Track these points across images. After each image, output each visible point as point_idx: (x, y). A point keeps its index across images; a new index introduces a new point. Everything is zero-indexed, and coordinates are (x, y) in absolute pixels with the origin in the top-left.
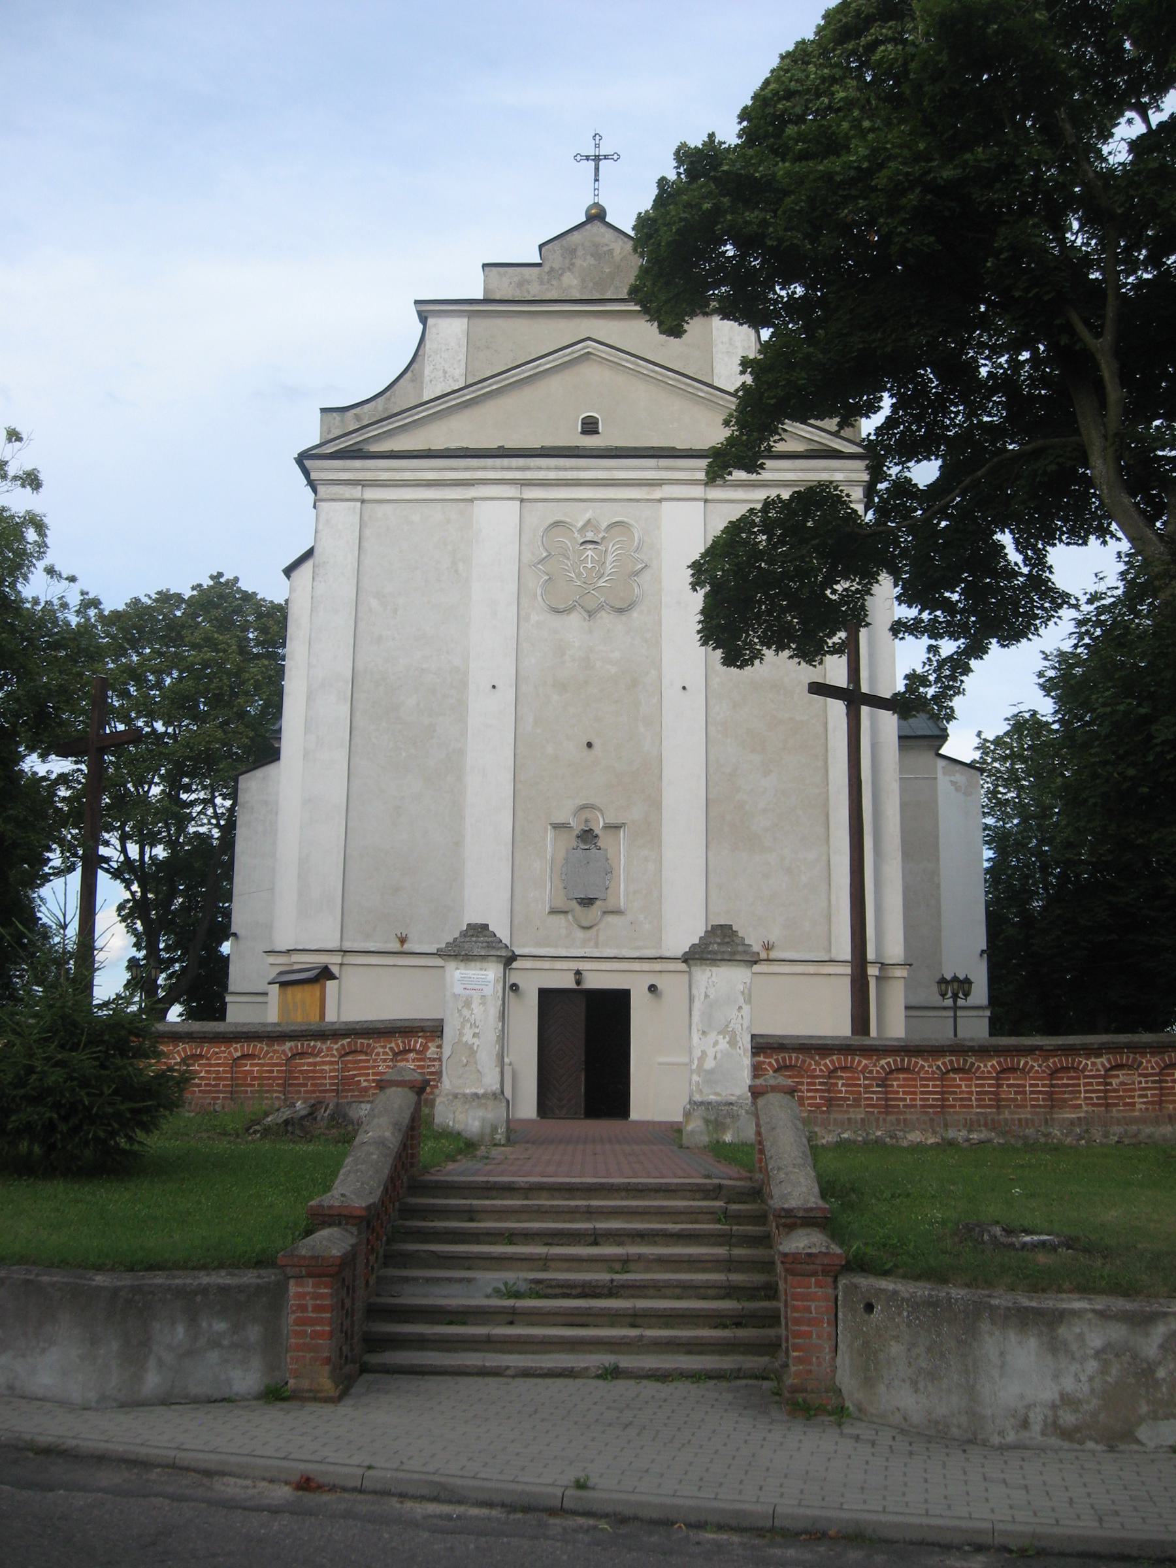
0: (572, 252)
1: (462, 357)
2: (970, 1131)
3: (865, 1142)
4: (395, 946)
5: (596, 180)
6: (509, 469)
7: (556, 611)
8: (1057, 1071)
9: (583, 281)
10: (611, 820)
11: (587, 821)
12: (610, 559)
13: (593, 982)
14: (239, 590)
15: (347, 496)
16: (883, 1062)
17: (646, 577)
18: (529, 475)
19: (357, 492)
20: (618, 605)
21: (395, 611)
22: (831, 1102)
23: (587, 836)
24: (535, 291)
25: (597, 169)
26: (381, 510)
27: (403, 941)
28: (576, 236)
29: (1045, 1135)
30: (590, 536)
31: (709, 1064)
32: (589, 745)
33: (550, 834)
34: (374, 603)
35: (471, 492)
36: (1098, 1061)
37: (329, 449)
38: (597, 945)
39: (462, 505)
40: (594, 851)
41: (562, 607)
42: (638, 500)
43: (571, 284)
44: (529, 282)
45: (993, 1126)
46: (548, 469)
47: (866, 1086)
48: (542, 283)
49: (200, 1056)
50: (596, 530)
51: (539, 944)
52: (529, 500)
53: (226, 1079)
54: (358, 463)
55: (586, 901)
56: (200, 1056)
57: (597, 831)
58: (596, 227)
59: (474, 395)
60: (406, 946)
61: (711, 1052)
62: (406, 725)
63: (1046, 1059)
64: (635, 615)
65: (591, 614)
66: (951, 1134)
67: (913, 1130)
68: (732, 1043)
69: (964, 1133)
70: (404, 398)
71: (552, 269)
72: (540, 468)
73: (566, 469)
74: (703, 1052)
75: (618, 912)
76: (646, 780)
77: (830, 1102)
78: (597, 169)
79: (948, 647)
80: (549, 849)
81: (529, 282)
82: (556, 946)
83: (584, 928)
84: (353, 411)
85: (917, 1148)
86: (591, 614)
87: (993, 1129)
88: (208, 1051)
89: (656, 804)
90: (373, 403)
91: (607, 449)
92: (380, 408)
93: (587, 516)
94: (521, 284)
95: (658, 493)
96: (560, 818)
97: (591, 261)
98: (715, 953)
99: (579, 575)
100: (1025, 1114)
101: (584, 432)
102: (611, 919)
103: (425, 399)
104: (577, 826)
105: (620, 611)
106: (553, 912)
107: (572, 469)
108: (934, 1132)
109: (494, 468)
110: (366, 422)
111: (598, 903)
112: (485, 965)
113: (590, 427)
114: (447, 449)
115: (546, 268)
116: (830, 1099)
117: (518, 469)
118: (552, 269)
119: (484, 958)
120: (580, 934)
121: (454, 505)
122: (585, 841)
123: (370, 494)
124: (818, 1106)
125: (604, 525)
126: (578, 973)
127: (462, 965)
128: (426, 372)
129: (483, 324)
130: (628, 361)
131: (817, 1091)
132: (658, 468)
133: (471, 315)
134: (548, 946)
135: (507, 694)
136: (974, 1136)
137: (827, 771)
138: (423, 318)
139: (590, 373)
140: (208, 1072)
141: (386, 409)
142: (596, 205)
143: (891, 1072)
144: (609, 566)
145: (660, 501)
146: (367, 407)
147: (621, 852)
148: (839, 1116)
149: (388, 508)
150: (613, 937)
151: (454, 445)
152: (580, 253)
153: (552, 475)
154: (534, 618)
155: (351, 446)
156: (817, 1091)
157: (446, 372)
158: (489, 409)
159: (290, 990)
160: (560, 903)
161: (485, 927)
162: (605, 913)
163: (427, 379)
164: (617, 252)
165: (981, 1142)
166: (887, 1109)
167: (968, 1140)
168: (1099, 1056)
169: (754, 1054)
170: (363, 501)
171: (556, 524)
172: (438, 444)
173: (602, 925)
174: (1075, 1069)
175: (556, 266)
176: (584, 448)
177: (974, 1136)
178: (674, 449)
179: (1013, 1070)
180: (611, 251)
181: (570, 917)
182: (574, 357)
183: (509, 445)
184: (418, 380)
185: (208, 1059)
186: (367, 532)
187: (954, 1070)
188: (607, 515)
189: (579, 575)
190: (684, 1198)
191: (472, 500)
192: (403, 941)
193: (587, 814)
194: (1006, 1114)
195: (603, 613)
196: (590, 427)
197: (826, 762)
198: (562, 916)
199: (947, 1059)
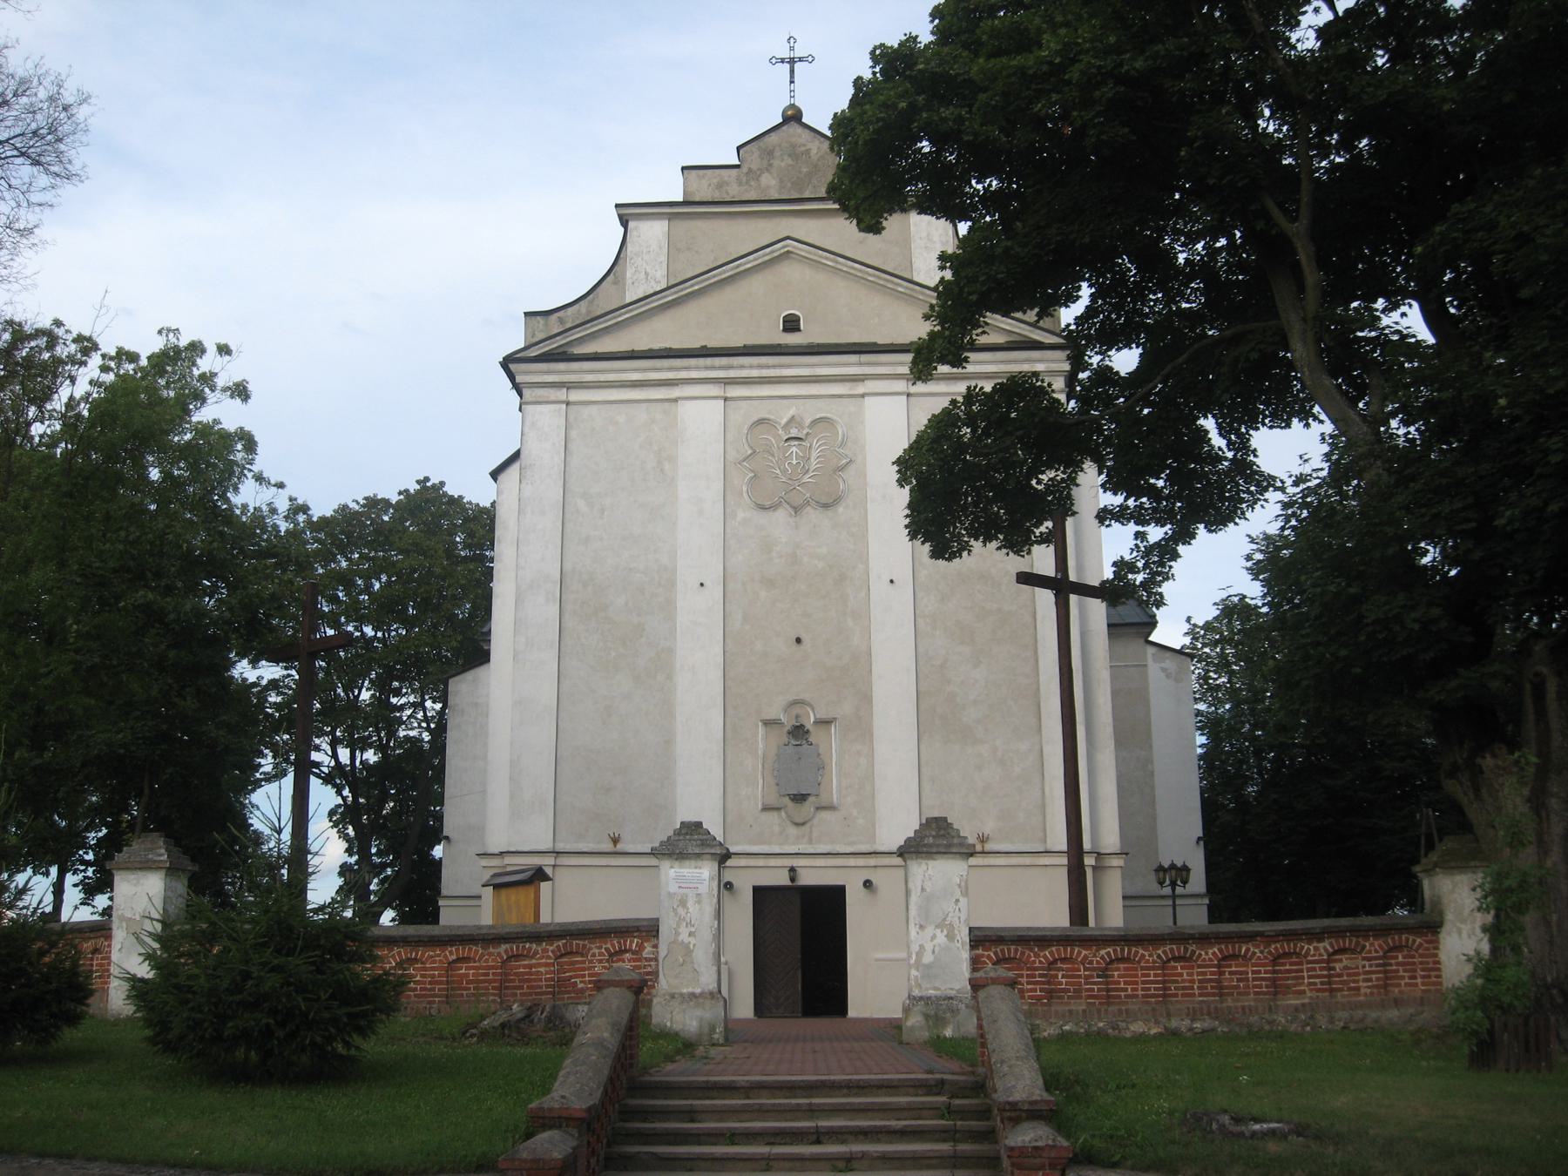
0: (769, 153)
1: (664, 258)
3: (1087, 1034)
4: (609, 847)
7: (763, 508)
9: (781, 181)
10: (822, 715)
12: (814, 454)
13: (808, 878)
15: (553, 398)
16: (1103, 952)
17: (851, 470)
18: (732, 374)
19: (562, 394)
20: (824, 500)
21: (602, 511)
23: (799, 732)
24: (734, 192)
25: (792, 71)
27: (615, 841)
28: (773, 137)
29: (1269, 1023)
30: (794, 432)
31: (928, 958)
32: (798, 640)
33: (761, 729)
34: (581, 504)
37: (534, 353)
38: (810, 842)
39: (666, 405)
43: (770, 184)
45: (1215, 1014)
46: (751, 367)
47: (1087, 977)
48: (740, 184)
49: (416, 960)
50: (800, 426)
51: (850, 844)
52: (575, 403)
53: (441, 983)
54: (562, 366)
55: (799, 797)
56: (416, 960)
58: (793, 128)
60: (620, 847)
61: (929, 947)
62: (615, 625)
64: (841, 509)
65: (797, 510)
68: (950, 937)
69: (1187, 1022)
70: (604, 303)
71: (750, 170)
72: (742, 367)
73: (768, 367)
74: (922, 947)
75: (831, 808)
76: (855, 674)
78: (792, 71)
79: (1155, 533)
83: (797, 824)
85: (1140, 1039)
86: (797, 510)
87: (1217, 1018)
89: (866, 699)
90: (576, 307)
92: (584, 311)
93: (792, 412)
94: (720, 186)
95: (860, 389)
98: (930, 846)
99: (784, 471)
100: (1249, 1001)
101: (785, 330)
102: (824, 815)
104: (788, 722)
105: (826, 506)
106: (766, 809)
107: (774, 367)
108: (1157, 1022)
109: (697, 368)
110: (569, 325)
111: (811, 799)
112: (700, 863)
113: (791, 324)
114: (651, 350)
115: (744, 169)
116: (1050, 992)
118: (750, 170)
119: (698, 856)
120: (793, 831)
121: (659, 406)
122: (796, 737)
123: (575, 396)
124: (1039, 998)
125: (808, 421)
126: (792, 870)
127: (677, 864)
128: (628, 275)
129: (683, 226)
136: (1197, 1025)
138: (624, 222)
139: (792, 272)
141: (589, 312)
142: (792, 106)
143: (1112, 961)
144: (813, 463)
145: (863, 396)
146: (570, 310)
147: (833, 745)
149: (593, 409)
150: (827, 833)
152: (777, 153)
153: (755, 373)
154: (741, 515)
155: (555, 350)
157: (649, 272)
158: (692, 310)
159: (504, 892)
160: (773, 800)
161: (699, 825)
162: (818, 808)
163: (629, 282)
165: (1204, 1031)
167: (1191, 1029)
168: (1320, 940)
169: (972, 947)
170: (568, 404)
171: (761, 421)
172: (642, 345)
173: (815, 821)
175: (754, 167)
176: (787, 346)
177: (1197, 1025)
179: (1234, 957)
182: (775, 257)
184: (620, 283)
186: (573, 434)
187: (1175, 959)
188: (810, 412)
189: (784, 471)
191: (676, 400)
192: (615, 841)
193: (796, 710)
196: (791, 324)
198: (775, 813)
199: (1167, 948)
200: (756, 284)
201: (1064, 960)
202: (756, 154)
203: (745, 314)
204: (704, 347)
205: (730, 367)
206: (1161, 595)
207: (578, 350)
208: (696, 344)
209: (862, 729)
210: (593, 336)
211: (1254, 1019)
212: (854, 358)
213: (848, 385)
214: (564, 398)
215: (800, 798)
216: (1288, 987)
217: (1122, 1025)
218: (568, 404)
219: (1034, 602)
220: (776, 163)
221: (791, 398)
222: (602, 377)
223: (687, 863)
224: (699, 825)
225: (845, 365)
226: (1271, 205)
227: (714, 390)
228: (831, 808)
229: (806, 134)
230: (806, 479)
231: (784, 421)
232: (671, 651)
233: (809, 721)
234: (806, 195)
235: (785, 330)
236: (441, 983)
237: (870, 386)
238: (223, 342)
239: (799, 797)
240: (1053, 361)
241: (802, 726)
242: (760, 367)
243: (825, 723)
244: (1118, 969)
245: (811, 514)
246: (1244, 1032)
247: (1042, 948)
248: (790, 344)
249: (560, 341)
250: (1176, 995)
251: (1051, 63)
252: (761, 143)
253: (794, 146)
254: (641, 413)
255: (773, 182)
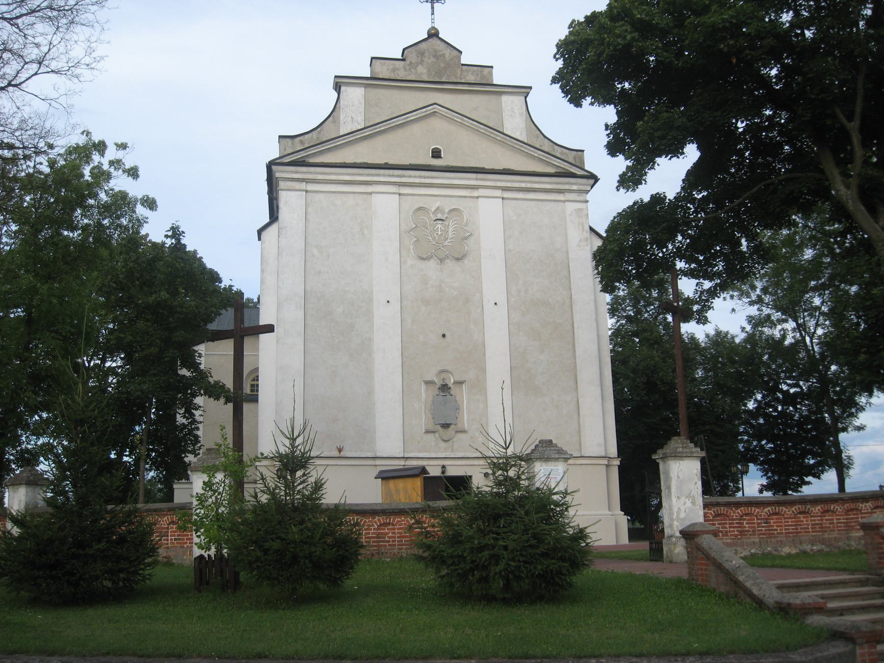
0: (422, 54)
1: (362, 110)
2: (812, 545)
3: (763, 554)
4: (336, 454)
5: (433, 14)
6: (393, 176)
7: (423, 259)
8: (848, 511)
9: (429, 71)
10: (458, 379)
11: (444, 379)
12: (451, 229)
13: (452, 472)
14: (150, 241)
15: (297, 188)
16: (766, 510)
17: (471, 240)
18: (404, 180)
19: (303, 186)
20: (457, 256)
21: (328, 256)
22: (742, 533)
23: (445, 388)
24: (402, 75)
25: (433, 8)
26: (318, 197)
27: (340, 450)
28: (424, 45)
29: (848, 546)
30: (439, 216)
31: (682, 515)
32: (444, 336)
33: (423, 387)
34: (315, 251)
35: (370, 189)
36: (867, 504)
37: (287, 160)
38: (452, 451)
39: (365, 196)
40: (448, 396)
41: (425, 256)
42: (465, 197)
43: (422, 72)
44: (398, 69)
45: (823, 542)
46: (415, 177)
47: (758, 524)
48: (406, 70)
49: (389, 524)
50: (443, 212)
51: (420, 451)
52: (311, 191)
53: (406, 537)
54: (304, 169)
55: (445, 425)
56: (389, 524)
57: (450, 385)
58: (434, 41)
59: (370, 132)
60: (342, 454)
61: (683, 509)
62: (337, 323)
63: (843, 505)
64: (466, 262)
65: (442, 260)
66: (808, 547)
67: (785, 546)
68: (693, 503)
69: (809, 547)
70: (328, 132)
71: (411, 63)
72: (410, 176)
73: (425, 177)
74: (679, 508)
75: (464, 431)
76: (476, 355)
77: (742, 533)
78: (433, 8)
79: (707, 285)
80: (424, 395)
81: (398, 69)
82: (429, 452)
83: (445, 441)
84: (299, 138)
85: (789, 555)
86: (442, 260)
87: (823, 544)
88: (394, 520)
89: (483, 370)
90: (310, 134)
91: (447, 167)
92: (315, 137)
93: (437, 204)
94: (394, 70)
95: (476, 193)
96: (428, 379)
97: (433, 59)
98: (682, 453)
99: (434, 238)
100: (835, 534)
101: (433, 157)
102: (460, 435)
103: (341, 134)
104: (439, 382)
105: (458, 259)
106: (427, 432)
107: (428, 177)
108: (796, 547)
109: (384, 175)
110: (307, 146)
111: (452, 426)
112: (557, 463)
113: (436, 154)
114: (355, 163)
115: (408, 62)
116: (741, 532)
117: (398, 176)
118: (411, 63)
119: (556, 459)
120: (443, 444)
121: (361, 196)
122: (443, 391)
123: (310, 187)
124: (736, 536)
125: (447, 210)
126: (444, 467)
127: (544, 464)
128: (341, 118)
129: (374, 92)
130: (458, 119)
131: (735, 527)
132: (477, 179)
133: (366, 86)
134: (425, 452)
135: (396, 306)
136: (815, 548)
137: (574, 351)
138: (337, 87)
139: (436, 123)
140: (394, 533)
141: (318, 138)
142: (433, 28)
143: (771, 514)
144: (450, 233)
145: (478, 197)
146: (306, 136)
147: (464, 396)
148: (748, 541)
149: (321, 196)
150: (462, 446)
151: (359, 161)
152: (427, 54)
153: (417, 180)
154: (409, 262)
155: (298, 159)
156: (735, 527)
157: (353, 117)
158: (379, 141)
159: (392, 483)
160: (431, 427)
161: (551, 441)
162: (457, 432)
163: (342, 122)
164: (447, 55)
165: (819, 551)
166: (770, 535)
167: (812, 550)
168: (867, 502)
169: (704, 508)
170: (307, 191)
171: (420, 209)
172: (350, 160)
173: (455, 439)
174: (857, 509)
175: (414, 61)
176: (434, 166)
177: (815, 548)
178: (484, 168)
179: (828, 511)
180: (444, 55)
181: (437, 435)
182: (427, 113)
183: (391, 162)
184: (336, 122)
185: (393, 525)
186: (310, 210)
187: (801, 513)
188: (448, 205)
189: (434, 238)
190: (852, 587)
191: (371, 193)
192: (340, 450)
193: (443, 375)
194: (826, 536)
195: (448, 261)
196: (436, 154)
197: (574, 346)
198: (432, 435)
199: (797, 507)
200: (416, 128)
201: (746, 515)
202: (415, 53)
203: (410, 146)
204: (386, 164)
205: (404, 176)
206: (706, 317)
207: (312, 160)
208: (382, 161)
209: (480, 386)
210: (321, 153)
211: (840, 544)
212: (474, 176)
213: (469, 191)
214: (304, 188)
215: (446, 426)
216: (853, 526)
217: (779, 549)
218: (307, 191)
219: (572, 318)
220: (426, 60)
221: (438, 196)
222: (328, 177)
223: (550, 463)
224: (551, 441)
225: (543, 183)
226: (838, 111)
227: (498, 193)
228: (464, 431)
229: (442, 45)
230: (446, 243)
231: (433, 209)
232: (370, 339)
233: (451, 382)
234: (443, 80)
235: (433, 157)
236: (406, 537)
237: (481, 192)
238: (605, 151)
239: (445, 425)
240: (581, 184)
241: (446, 385)
242: (420, 177)
243: (460, 383)
244: (745, 519)
245: (449, 263)
246: (837, 551)
247: (737, 508)
248: (435, 165)
249: (303, 154)
250: (749, 531)
251: (731, 23)
252: (417, 48)
253: (436, 51)
254: (350, 200)
255: (425, 71)
